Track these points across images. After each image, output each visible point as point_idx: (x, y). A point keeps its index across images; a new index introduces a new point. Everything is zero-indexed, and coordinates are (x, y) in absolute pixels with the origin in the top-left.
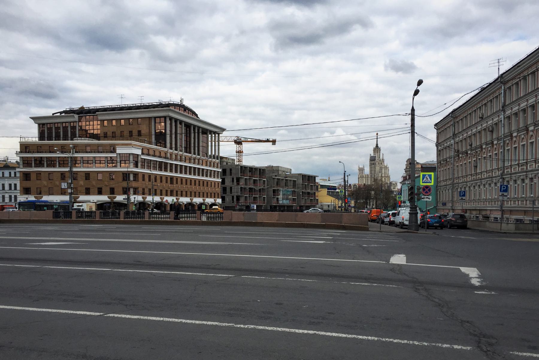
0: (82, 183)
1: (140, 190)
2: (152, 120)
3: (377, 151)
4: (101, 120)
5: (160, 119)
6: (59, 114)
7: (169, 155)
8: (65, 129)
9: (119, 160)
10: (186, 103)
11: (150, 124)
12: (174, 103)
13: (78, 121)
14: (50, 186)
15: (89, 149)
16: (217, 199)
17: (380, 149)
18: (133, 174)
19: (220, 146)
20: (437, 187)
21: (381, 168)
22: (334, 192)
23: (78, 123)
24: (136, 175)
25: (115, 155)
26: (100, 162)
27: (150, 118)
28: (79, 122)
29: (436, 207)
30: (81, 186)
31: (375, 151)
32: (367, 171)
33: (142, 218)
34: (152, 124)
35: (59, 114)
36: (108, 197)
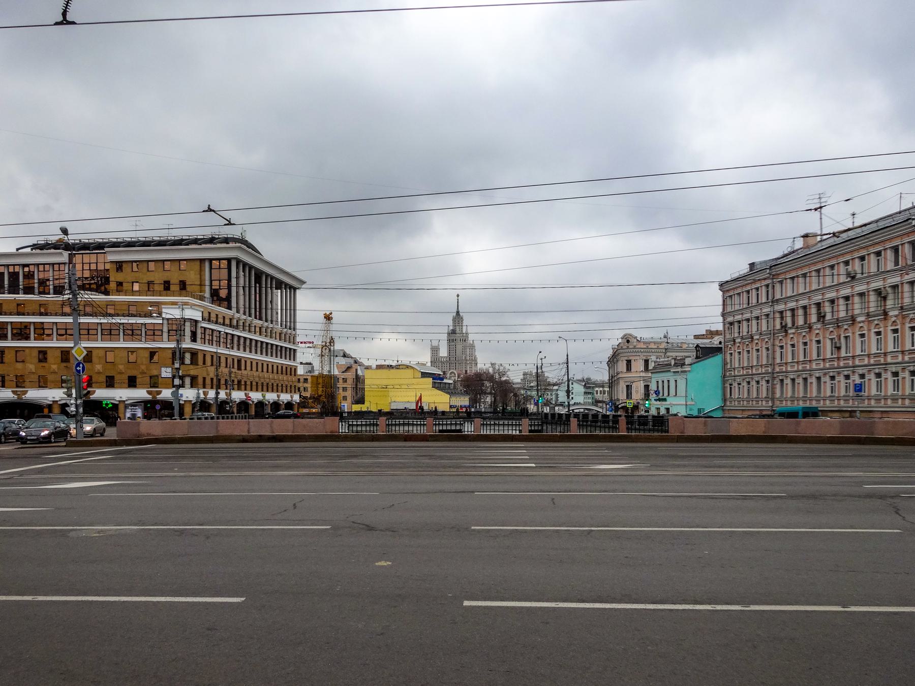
0: (32, 367)
1: (200, 380)
2: (205, 263)
3: (458, 321)
4: (111, 262)
5: (59, 266)
6: (28, 250)
7: (235, 322)
8: (14, 276)
9: (165, 329)
10: (249, 238)
11: (201, 270)
12: (235, 236)
13: (68, 262)
14: (42, 373)
15: (135, 310)
16: (267, 394)
17: (462, 318)
18: (191, 353)
19: (721, 304)
20: (724, 377)
21: (464, 348)
22: (440, 383)
23: (68, 265)
24: (194, 354)
25: (161, 322)
26: (154, 333)
27: (202, 261)
28: (69, 264)
29: (723, 407)
30: (99, 373)
31: (455, 321)
32: (443, 352)
33: (607, 430)
34: (205, 269)
35: (28, 250)
36: (14, 392)
